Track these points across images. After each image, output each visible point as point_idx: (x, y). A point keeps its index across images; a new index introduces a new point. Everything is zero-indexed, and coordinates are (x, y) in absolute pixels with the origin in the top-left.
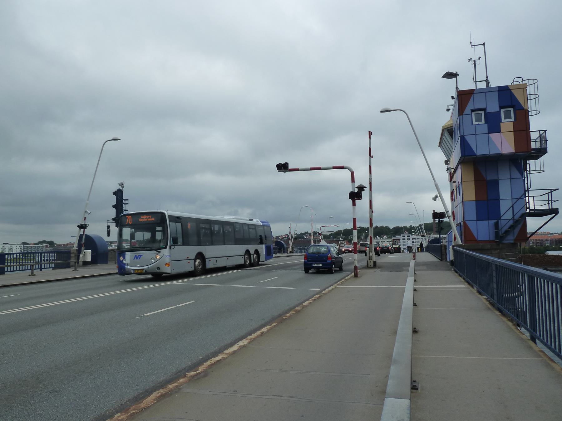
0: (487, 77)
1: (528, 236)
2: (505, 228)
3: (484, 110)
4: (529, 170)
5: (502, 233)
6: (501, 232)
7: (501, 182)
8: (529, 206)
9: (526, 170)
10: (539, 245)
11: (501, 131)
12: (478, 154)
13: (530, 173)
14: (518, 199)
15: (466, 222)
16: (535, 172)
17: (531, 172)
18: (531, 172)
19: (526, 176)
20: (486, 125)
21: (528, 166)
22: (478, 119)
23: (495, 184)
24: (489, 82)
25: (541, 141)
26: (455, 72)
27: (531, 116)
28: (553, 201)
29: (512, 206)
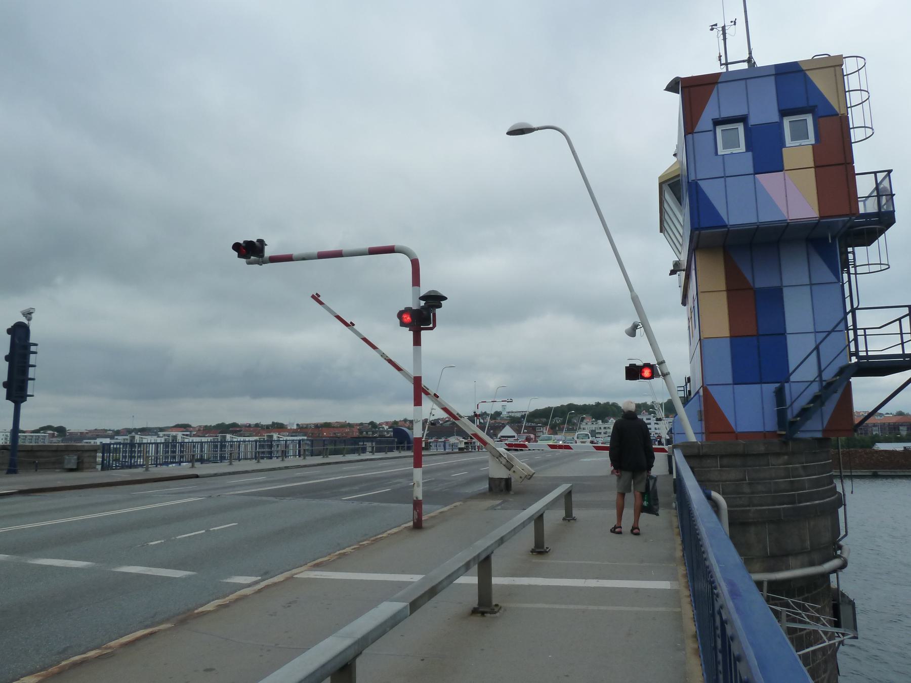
0: (750, 53)
1: (857, 420)
2: (802, 402)
3: (743, 119)
5: (794, 415)
6: (792, 413)
9: (846, 264)
10: (861, 433)
11: (786, 168)
12: (731, 223)
13: (856, 274)
14: (829, 333)
16: (865, 269)
20: (750, 154)
21: (851, 256)
23: (775, 296)
25: (879, 196)
29: (817, 348)
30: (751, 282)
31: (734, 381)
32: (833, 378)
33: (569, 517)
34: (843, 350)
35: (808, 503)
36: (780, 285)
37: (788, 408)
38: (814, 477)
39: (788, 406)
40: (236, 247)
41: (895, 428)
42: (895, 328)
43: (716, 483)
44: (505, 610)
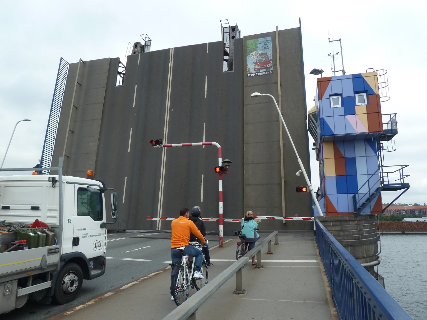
0: (343, 68)
1: (383, 208)
2: (363, 201)
3: (341, 94)
4: (382, 149)
5: (360, 206)
7: (357, 160)
9: (379, 149)
13: (383, 152)
16: (387, 150)
17: (385, 151)
18: (385, 151)
19: (379, 154)
20: (343, 108)
21: (381, 145)
22: (336, 103)
23: (353, 161)
25: (392, 123)
28: (404, 177)
29: (368, 181)
30: (343, 155)
31: (337, 191)
32: (374, 192)
33: (276, 243)
35: (365, 239)
36: (354, 156)
38: (367, 229)
39: (357, 202)
41: (413, 211)
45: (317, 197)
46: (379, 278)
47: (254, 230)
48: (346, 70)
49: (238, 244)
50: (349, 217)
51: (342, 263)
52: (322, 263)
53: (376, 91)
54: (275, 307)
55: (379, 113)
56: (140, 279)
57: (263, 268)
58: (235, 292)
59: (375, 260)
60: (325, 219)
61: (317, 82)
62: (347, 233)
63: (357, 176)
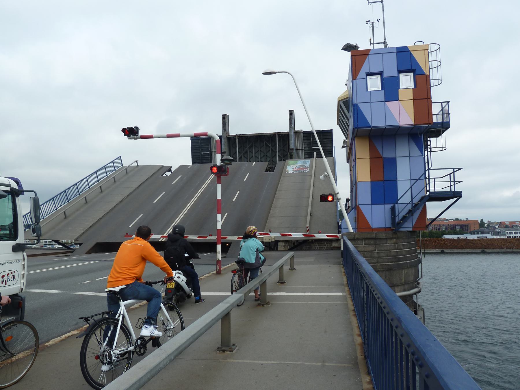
0: (385, 39)
1: (428, 222)
2: (403, 213)
3: (380, 74)
4: (430, 147)
8: (429, 189)
9: (426, 147)
13: (431, 151)
14: (417, 180)
15: (359, 205)
16: (435, 149)
17: (432, 150)
18: (432, 150)
19: (426, 154)
20: (383, 91)
21: (429, 143)
23: (392, 162)
24: (387, 44)
25: (443, 114)
26: (355, 44)
27: (433, 86)
28: (456, 183)
29: (411, 188)
33: (292, 268)
34: (424, 188)
35: (404, 262)
36: (395, 156)
37: (396, 217)
40: (124, 130)
41: (454, 227)
42: (447, 178)
43: (362, 252)
44: (272, 304)
45: (347, 210)
46: (418, 309)
47: (255, 252)
48: (388, 41)
49: (234, 272)
50: (385, 233)
51: (374, 295)
52: (350, 297)
53: (426, 71)
54: (276, 377)
55: (429, 99)
56: (84, 327)
57: (268, 305)
58: (219, 349)
59: (416, 288)
60: (356, 236)
61: (351, 56)
62: (382, 254)
63: (398, 181)
